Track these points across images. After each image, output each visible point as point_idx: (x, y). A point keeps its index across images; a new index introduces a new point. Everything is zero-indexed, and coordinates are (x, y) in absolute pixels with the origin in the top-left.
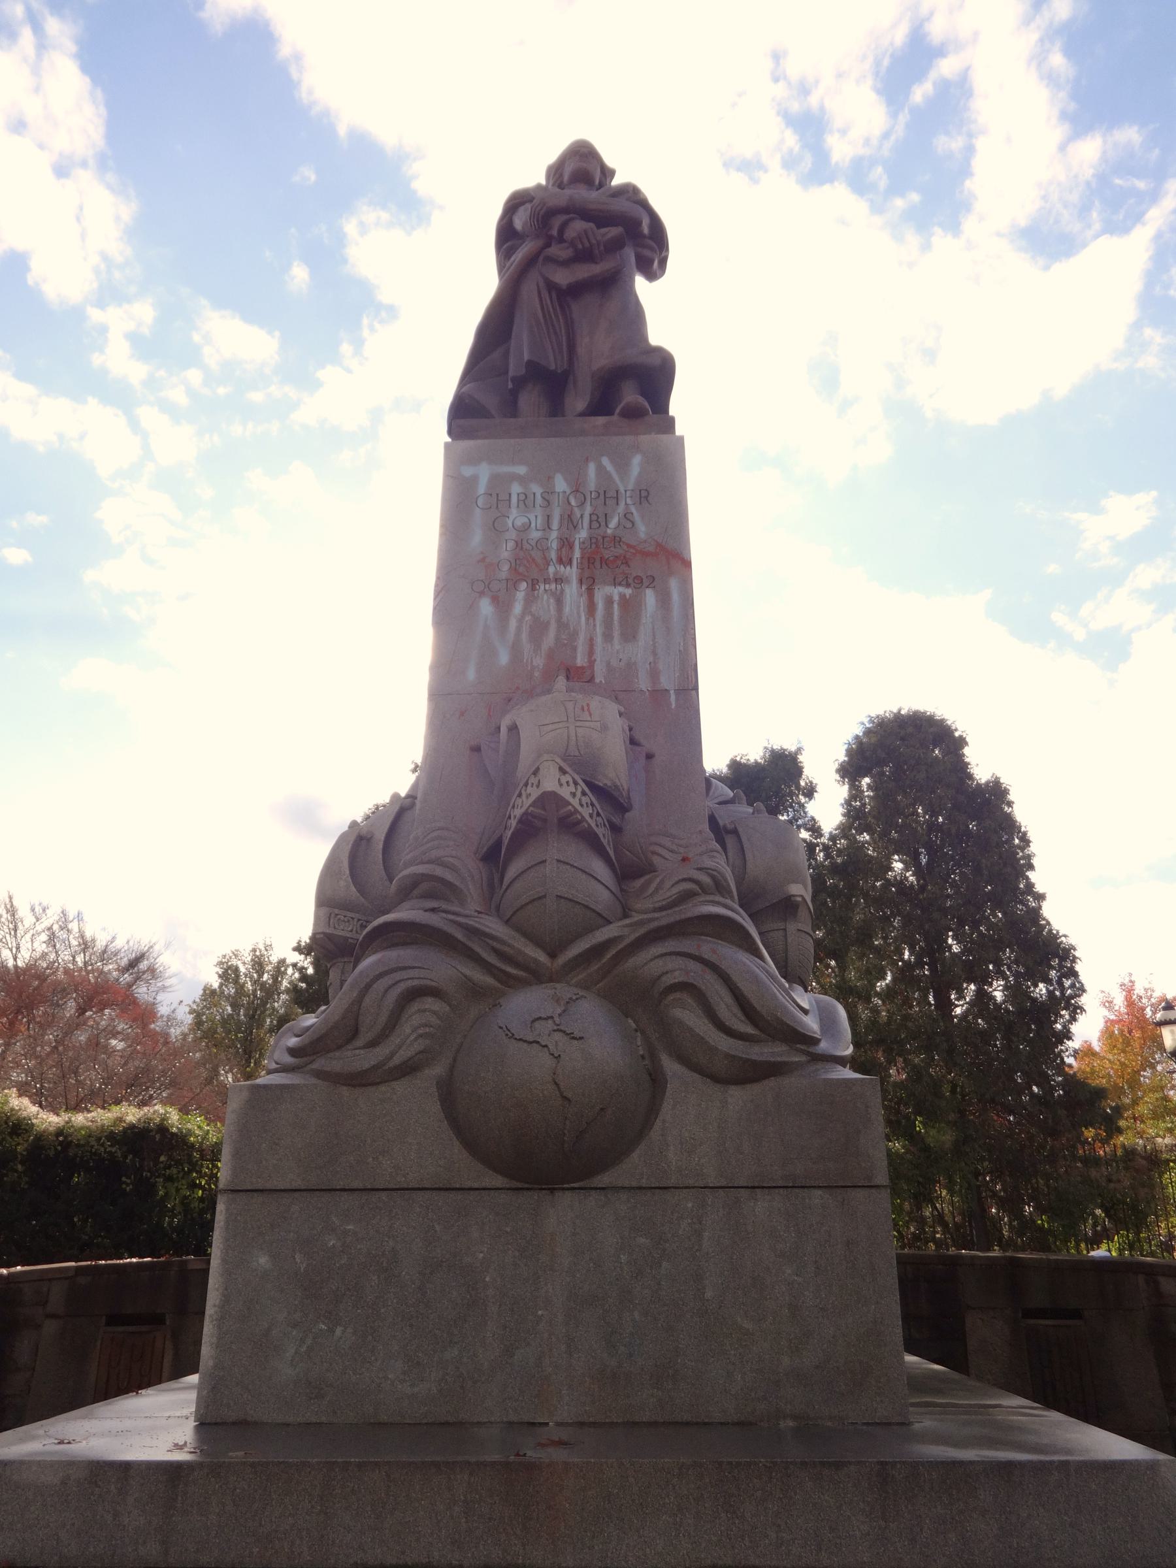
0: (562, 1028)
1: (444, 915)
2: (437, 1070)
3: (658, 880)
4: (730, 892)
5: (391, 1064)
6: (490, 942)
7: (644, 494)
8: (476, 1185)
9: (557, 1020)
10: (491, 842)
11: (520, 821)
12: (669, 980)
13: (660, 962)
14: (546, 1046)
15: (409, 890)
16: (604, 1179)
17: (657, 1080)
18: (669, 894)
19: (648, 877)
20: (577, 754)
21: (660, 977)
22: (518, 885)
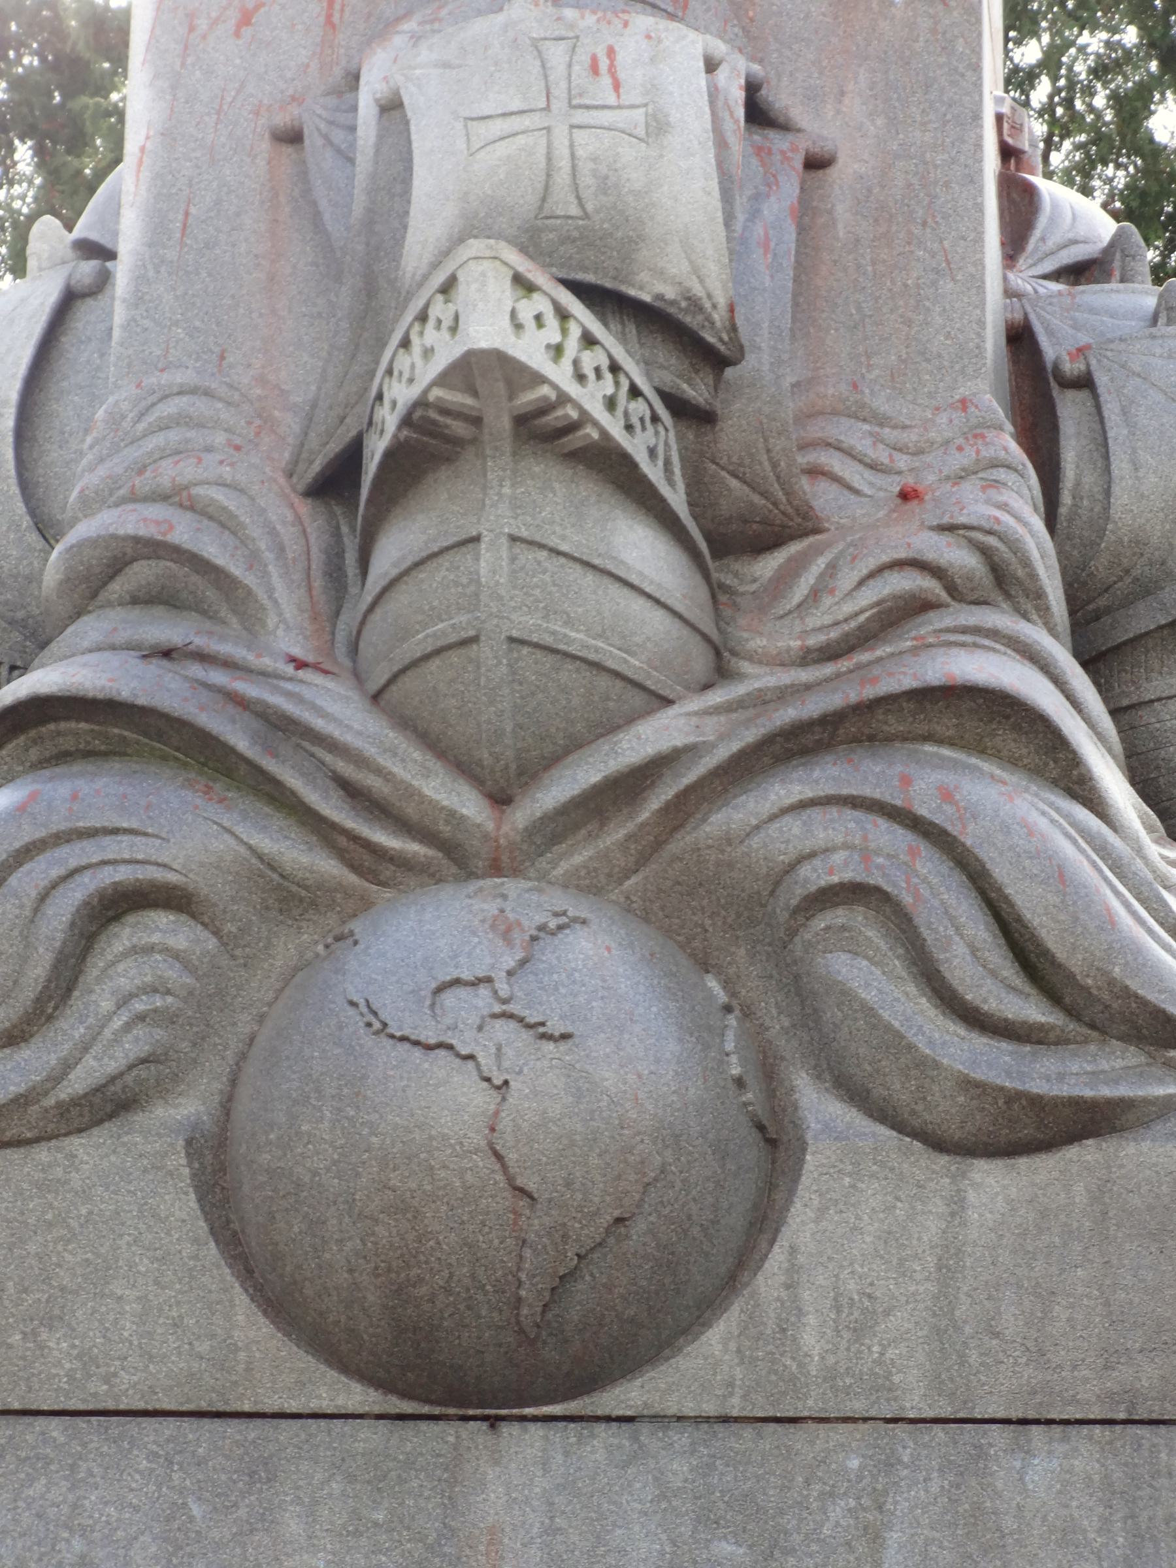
0: (511, 1008)
1: (196, 670)
2: (188, 1107)
3: (821, 563)
4: (1038, 595)
5: (64, 1093)
6: (328, 758)
8: (293, 1406)
9: (503, 989)
10: (334, 447)
11: (407, 421)
12: (815, 876)
13: (793, 826)
14: (471, 1057)
15: (102, 576)
16: (611, 1400)
17: (776, 1142)
18: (848, 608)
19: (794, 548)
20: (574, 210)
21: (792, 867)
22: (401, 600)
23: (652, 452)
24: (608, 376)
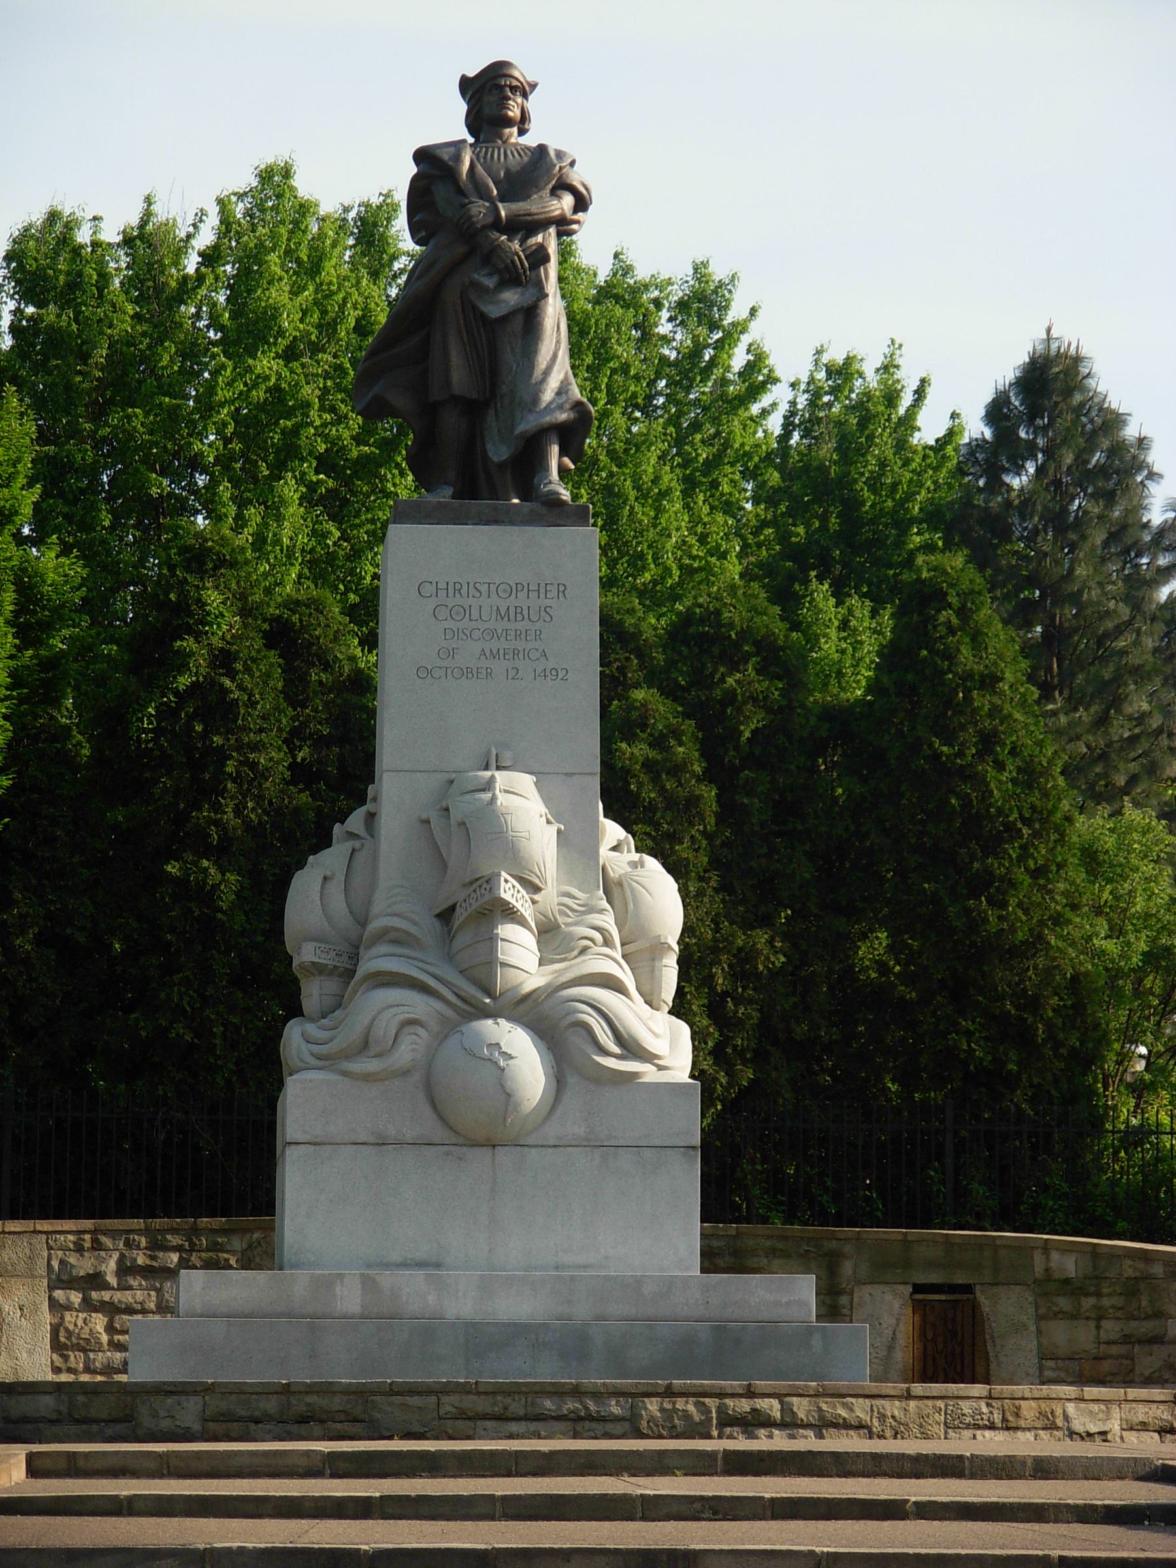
7: (562, 588)
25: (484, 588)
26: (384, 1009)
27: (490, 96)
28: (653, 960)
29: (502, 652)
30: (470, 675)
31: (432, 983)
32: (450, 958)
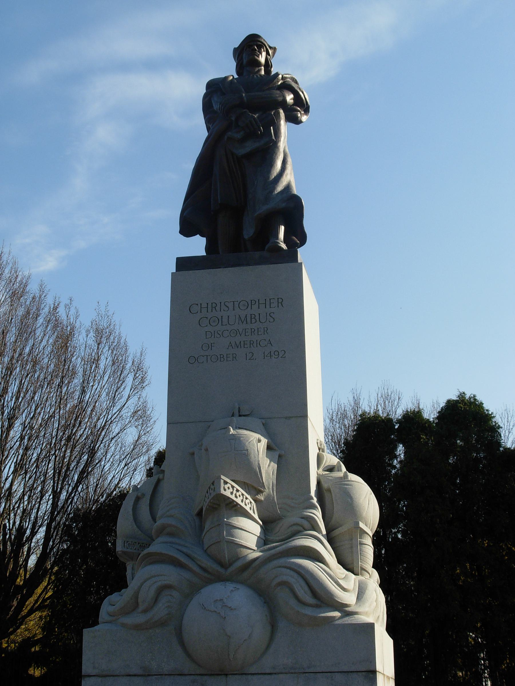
7: (280, 301)
23: (250, 508)
24: (241, 496)
25: (230, 305)
26: (145, 582)
27: (250, 48)
28: (352, 540)
29: (242, 343)
30: (222, 359)
31: (183, 559)
32: (200, 543)
